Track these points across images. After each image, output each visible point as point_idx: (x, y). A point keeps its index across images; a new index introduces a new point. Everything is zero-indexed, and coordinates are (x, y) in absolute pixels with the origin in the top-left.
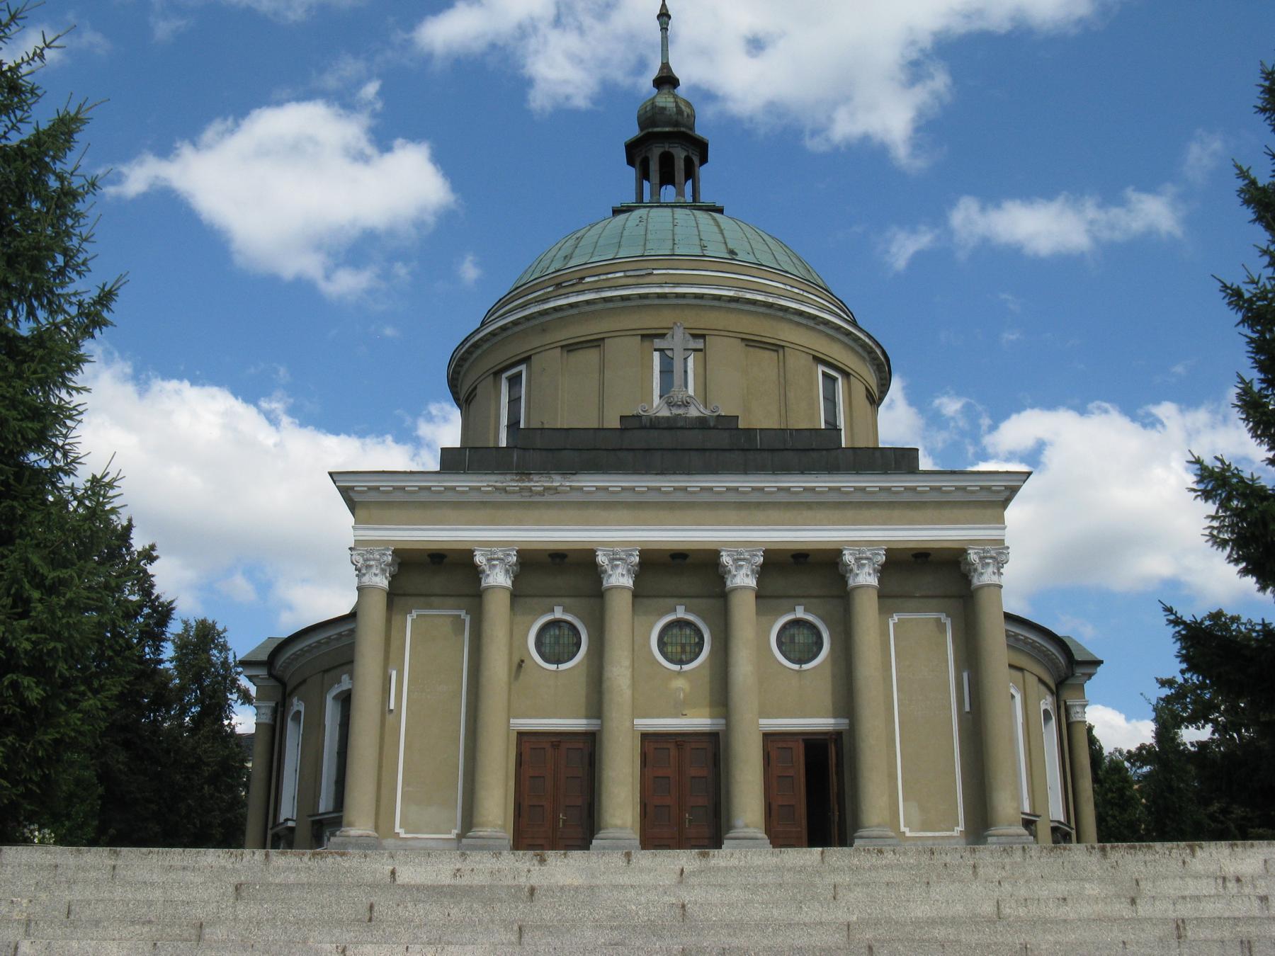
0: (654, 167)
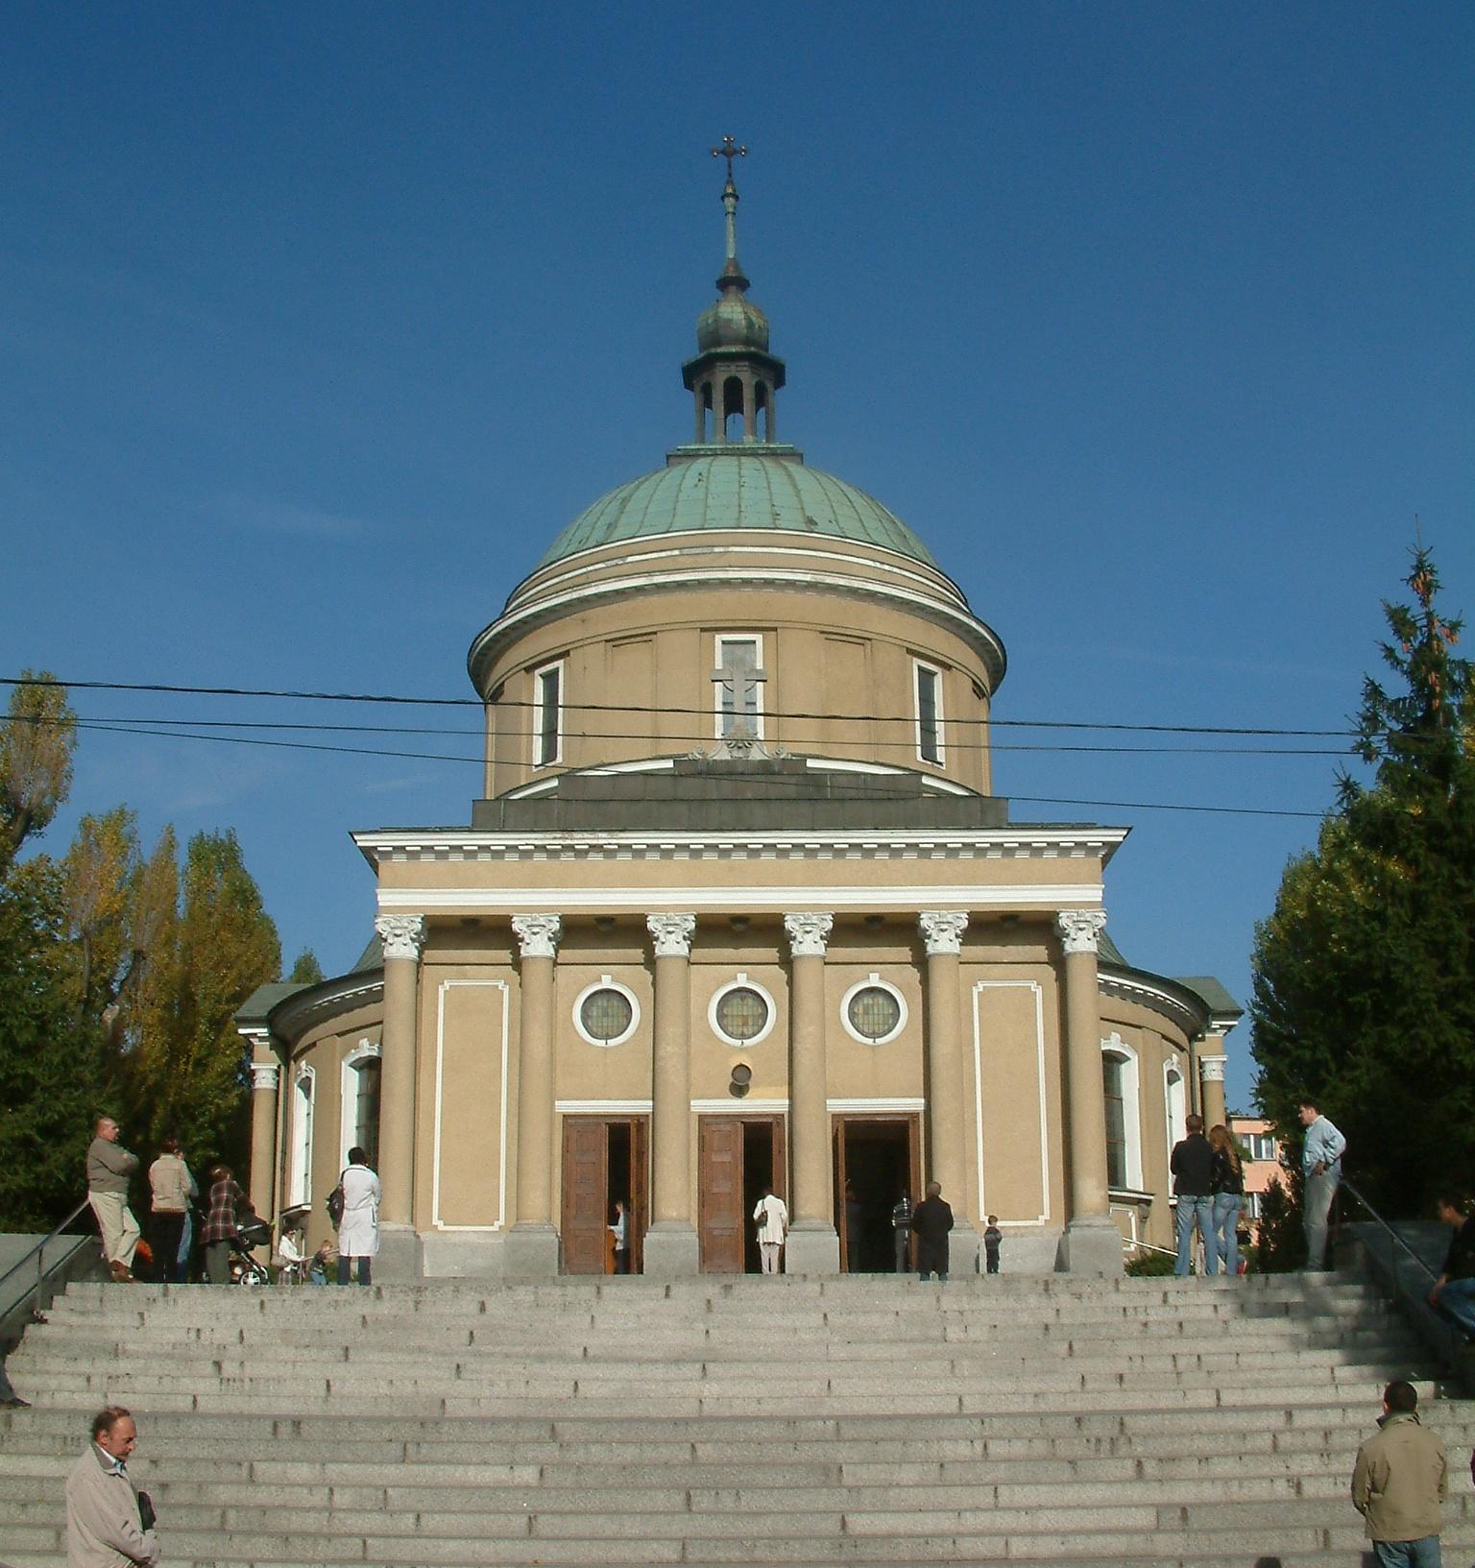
0: (718, 396)
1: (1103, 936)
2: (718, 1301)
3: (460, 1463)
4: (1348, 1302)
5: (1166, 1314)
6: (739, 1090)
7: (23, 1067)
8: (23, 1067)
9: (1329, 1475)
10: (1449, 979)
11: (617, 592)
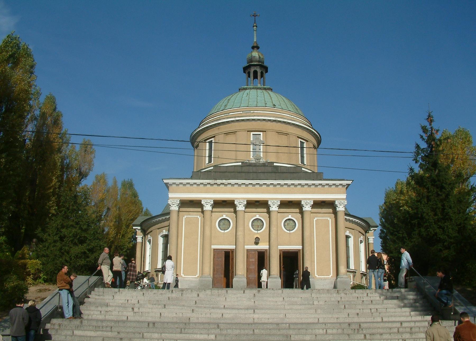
1: (346, 207)
2: (257, 294)
3: (195, 334)
4: (411, 296)
5: (368, 299)
6: (257, 243)
7: (84, 234)
8: (84, 234)
9: (412, 338)
10: (436, 217)
11: (227, 122)
